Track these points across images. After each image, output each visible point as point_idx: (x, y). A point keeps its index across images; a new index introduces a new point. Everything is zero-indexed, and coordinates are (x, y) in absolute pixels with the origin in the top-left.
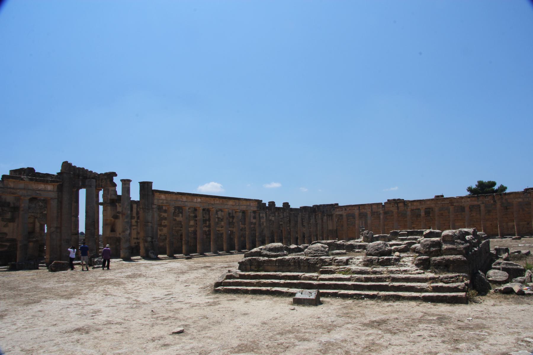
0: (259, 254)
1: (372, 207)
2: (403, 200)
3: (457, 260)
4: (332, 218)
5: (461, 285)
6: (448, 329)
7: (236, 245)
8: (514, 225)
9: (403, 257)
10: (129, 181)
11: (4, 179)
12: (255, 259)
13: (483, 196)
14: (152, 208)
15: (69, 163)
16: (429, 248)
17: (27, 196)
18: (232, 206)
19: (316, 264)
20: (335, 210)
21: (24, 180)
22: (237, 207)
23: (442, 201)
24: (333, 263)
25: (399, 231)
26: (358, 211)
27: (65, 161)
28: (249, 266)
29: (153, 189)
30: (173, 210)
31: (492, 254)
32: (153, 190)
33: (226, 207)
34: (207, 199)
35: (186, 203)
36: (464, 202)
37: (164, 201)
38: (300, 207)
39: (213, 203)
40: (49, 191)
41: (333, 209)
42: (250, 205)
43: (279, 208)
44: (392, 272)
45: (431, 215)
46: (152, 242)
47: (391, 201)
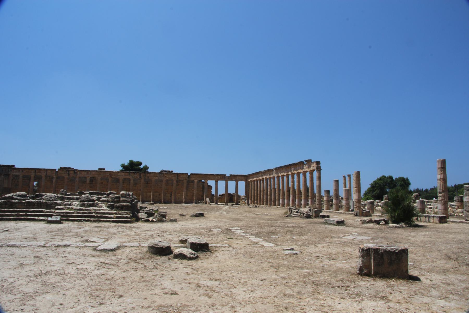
0: (11, 198)
2: (73, 168)
3: (127, 205)
5: (129, 216)
8: (151, 195)
9: (99, 204)
12: (10, 201)
13: (133, 172)
16: (114, 199)
19: (52, 205)
23: (104, 173)
24: (62, 205)
25: (84, 191)
26: (34, 174)
28: (4, 205)
31: (138, 209)
36: (120, 175)
44: (95, 210)
45: (94, 183)
47: (63, 168)
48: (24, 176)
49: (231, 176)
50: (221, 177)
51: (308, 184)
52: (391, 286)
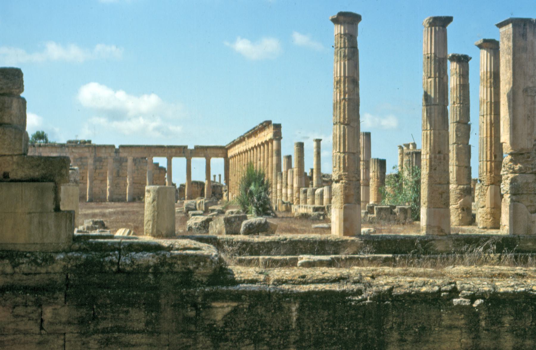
49: (197, 148)
50: (178, 151)
51: (270, 159)
52: (468, 275)
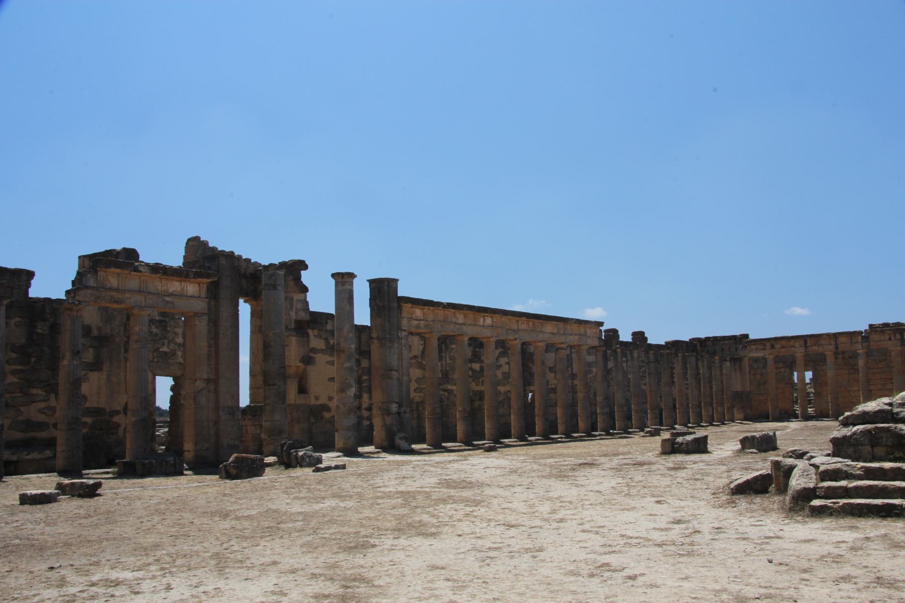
1: (836, 341)
4: (740, 367)
6: (170, 572)
7: (559, 421)
10: (352, 276)
11: (98, 269)
14: (399, 338)
15: (203, 242)
17: (146, 307)
18: (551, 335)
20: (748, 347)
21: (140, 272)
22: (562, 339)
26: (803, 350)
27: (194, 236)
28: (869, 448)
29: (399, 295)
30: (421, 344)
32: (400, 297)
33: (541, 336)
34: (505, 319)
35: (465, 327)
37: (421, 322)
38: (665, 343)
39: (515, 327)
40: (191, 296)
41: (743, 346)
42: (585, 335)
43: (625, 344)
46: (399, 413)
47: (878, 327)
48: (778, 360)
